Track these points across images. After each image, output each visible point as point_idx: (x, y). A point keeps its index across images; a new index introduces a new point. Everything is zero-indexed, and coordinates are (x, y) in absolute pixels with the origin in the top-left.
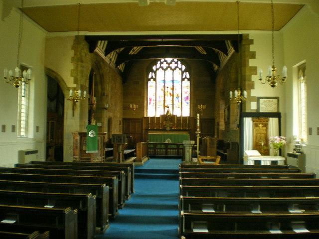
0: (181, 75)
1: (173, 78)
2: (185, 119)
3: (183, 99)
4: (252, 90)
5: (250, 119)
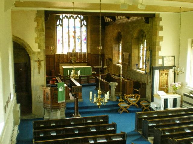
0: (80, 23)
1: (75, 25)
2: (85, 55)
3: (82, 40)
4: (160, 52)
5: (158, 70)
